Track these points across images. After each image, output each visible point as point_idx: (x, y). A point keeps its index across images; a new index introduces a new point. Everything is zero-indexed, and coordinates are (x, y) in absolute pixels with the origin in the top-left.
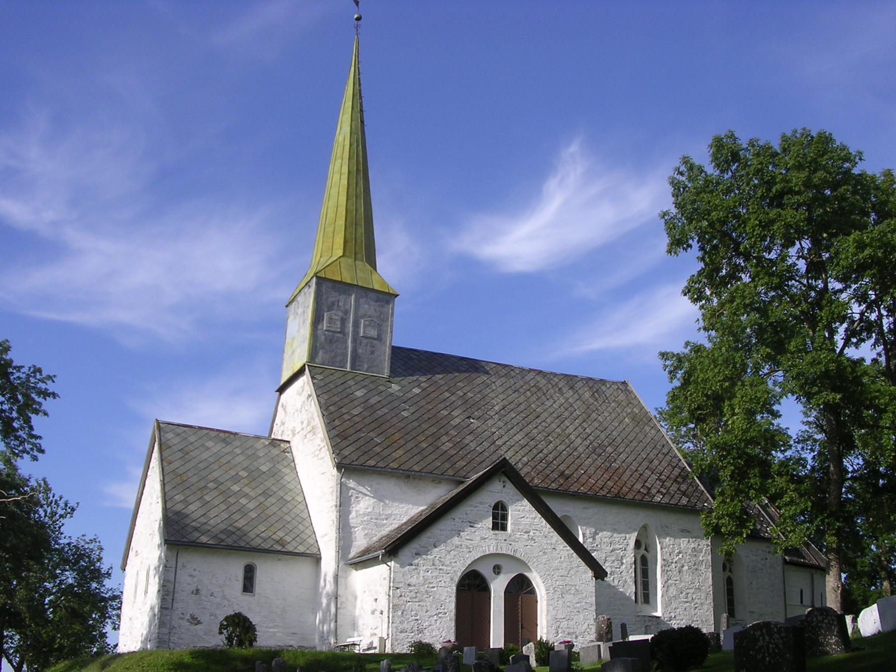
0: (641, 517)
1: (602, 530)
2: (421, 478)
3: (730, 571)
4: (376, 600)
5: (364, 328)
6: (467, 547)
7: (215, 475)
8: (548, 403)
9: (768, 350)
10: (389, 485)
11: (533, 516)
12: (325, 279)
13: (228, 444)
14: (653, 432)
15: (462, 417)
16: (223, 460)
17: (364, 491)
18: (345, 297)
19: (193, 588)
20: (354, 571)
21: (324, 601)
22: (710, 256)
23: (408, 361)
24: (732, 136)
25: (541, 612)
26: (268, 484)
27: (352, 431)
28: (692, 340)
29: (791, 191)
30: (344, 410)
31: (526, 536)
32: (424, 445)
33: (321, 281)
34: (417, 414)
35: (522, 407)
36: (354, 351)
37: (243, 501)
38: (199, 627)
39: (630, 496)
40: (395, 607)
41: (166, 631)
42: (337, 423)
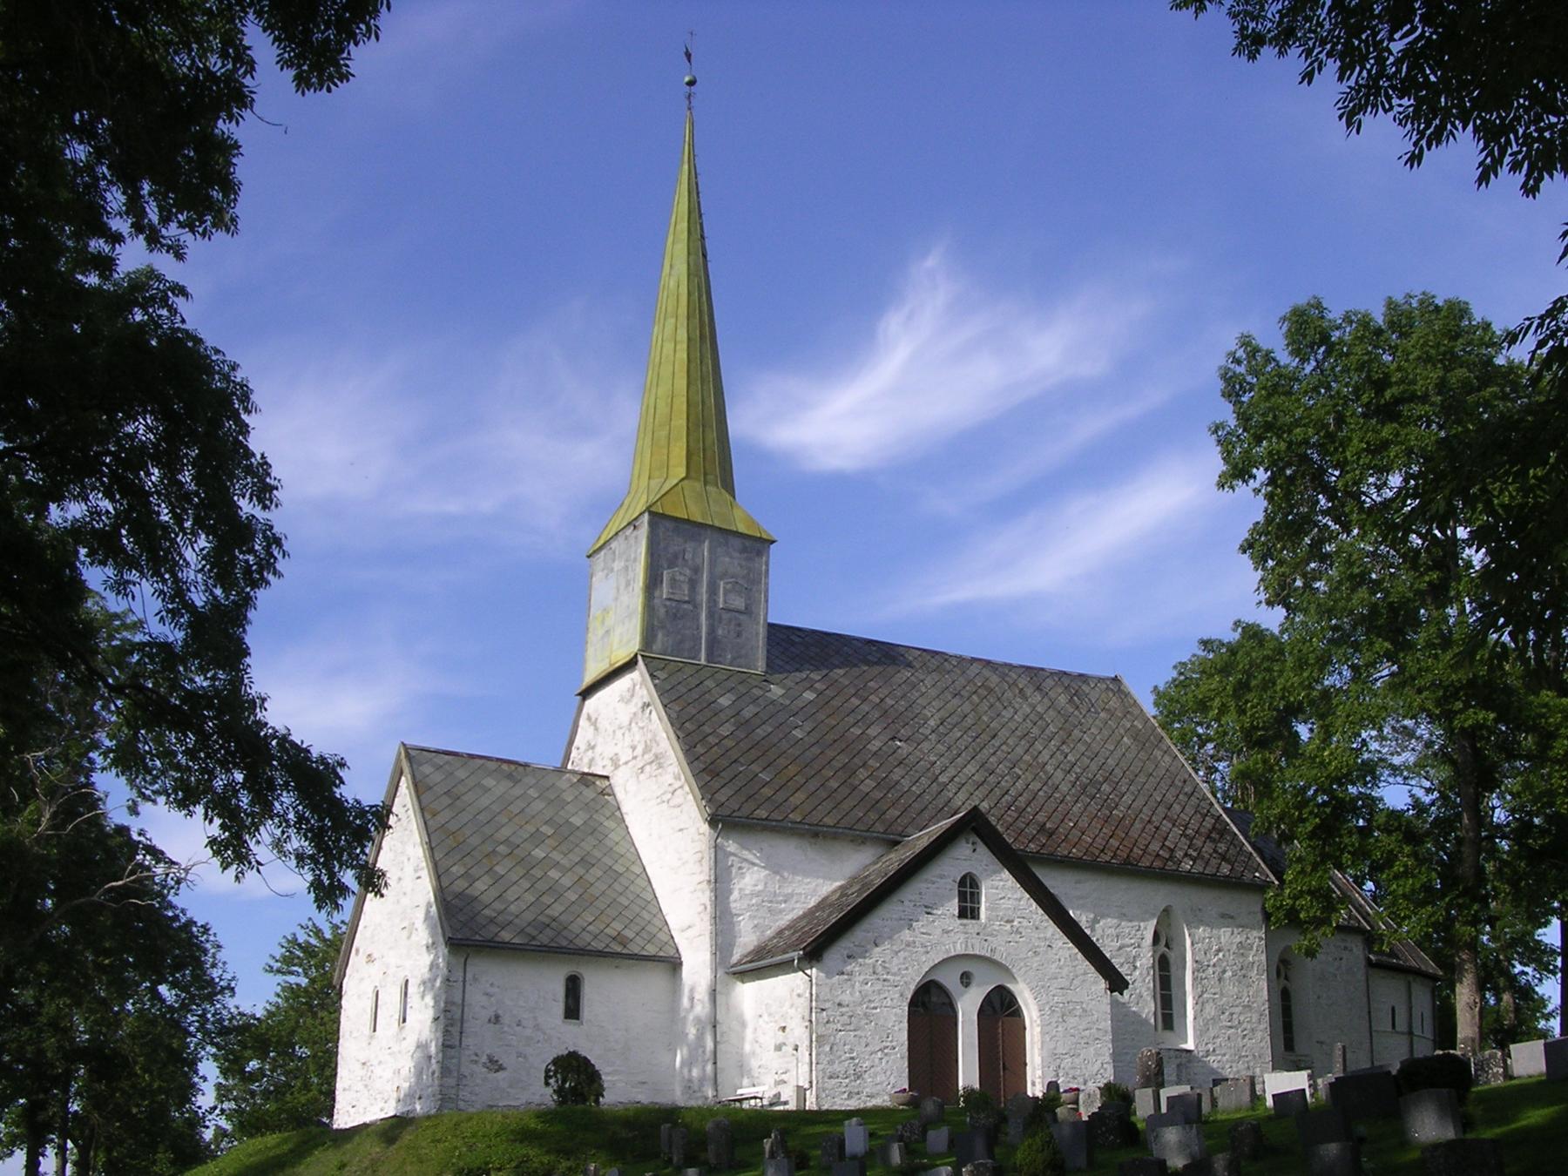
0: (1160, 895)
1: (1103, 917)
2: (835, 837)
3: (1286, 978)
4: (784, 1029)
5: (725, 594)
6: (923, 946)
7: (505, 832)
8: (1007, 714)
9: (1387, 644)
10: (787, 849)
11: (1018, 895)
12: (664, 516)
13: (517, 782)
14: (1167, 758)
15: (884, 738)
16: (515, 809)
17: (750, 857)
18: (701, 541)
19: (491, 1013)
20: (739, 984)
21: (692, 1032)
22: (1281, 492)
23: (797, 648)
24: (1318, 305)
25: (1032, 1043)
26: (587, 846)
27: (724, 762)
28: (1249, 619)
29: (1413, 398)
30: (707, 729)
31: (1008, 926)
32: (834, 784)
33: (657, 518)
34: (818, 733)
35: (969, 721)
36: (712, 631)
37: (554, 874)
38: (500, 1075)
39: (1145, 863)
40: (821, 1039)
41: (451, 1081)
42: (700, 749)
